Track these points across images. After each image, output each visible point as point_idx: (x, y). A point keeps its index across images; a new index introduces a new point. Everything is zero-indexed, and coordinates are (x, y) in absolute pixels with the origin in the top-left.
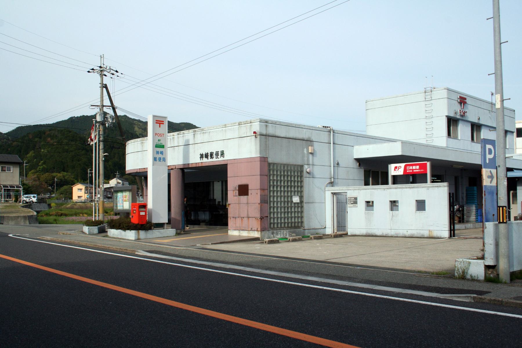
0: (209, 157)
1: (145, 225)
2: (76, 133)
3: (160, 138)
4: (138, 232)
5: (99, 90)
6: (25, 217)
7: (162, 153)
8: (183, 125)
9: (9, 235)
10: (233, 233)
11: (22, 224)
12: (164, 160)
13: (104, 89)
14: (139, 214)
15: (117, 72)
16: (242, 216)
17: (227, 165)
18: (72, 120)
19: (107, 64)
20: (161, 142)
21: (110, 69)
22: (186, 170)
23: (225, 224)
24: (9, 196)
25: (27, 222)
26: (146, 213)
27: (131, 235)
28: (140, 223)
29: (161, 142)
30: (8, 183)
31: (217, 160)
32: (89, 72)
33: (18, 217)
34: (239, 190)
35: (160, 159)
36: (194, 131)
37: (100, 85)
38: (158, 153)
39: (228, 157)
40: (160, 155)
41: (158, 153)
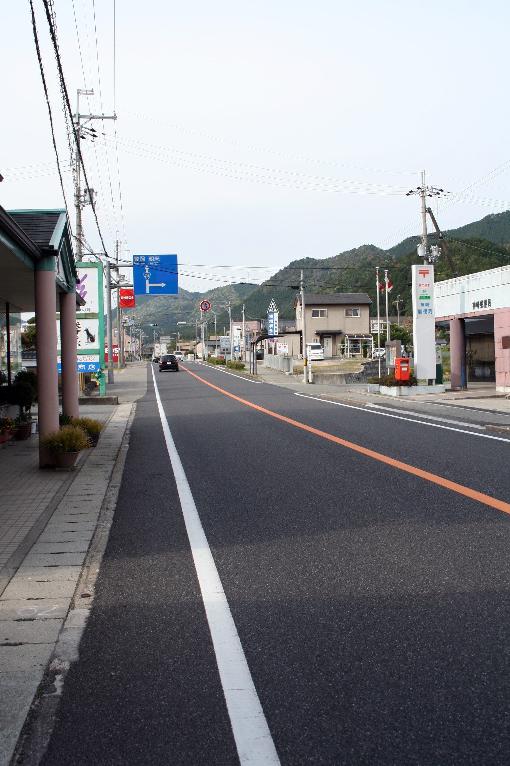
0: (480, 306)
1: (410, 381)
2: (490, 243)
3: (424, 289)
4: (400, 388)
5: (422, 215)
6: (341, 376)
7: (428, 304)
8: (337, 258)
9: (167, 363)
10: (500, 390)
11: (338, 384)
12: (431, 311)
13: (428, 214)
14: (401, 369)
15: (442, 190)
16: (506, 371)
17: (492, 315)
18: (489, 220)
19: (429, 183)
20: (426, 293)
21: (432, 188)
22: (466, 320)
23: (492, 378)
24: (357, 349)
25: (344, 381)
26: (408, 369)
27: (393, 391)
28: (402, 379)
29: (426, 293)
30: (355, 332)
31: (486, 309)
32: (408, 195)
33: (334, 375)
34: (503, 342)
35: (425, 311)
36: (468, 277)
37: (422, 210)
38: (422, 304)
39: (495, 306)
40: (425, 307)
41: (422, 304)
